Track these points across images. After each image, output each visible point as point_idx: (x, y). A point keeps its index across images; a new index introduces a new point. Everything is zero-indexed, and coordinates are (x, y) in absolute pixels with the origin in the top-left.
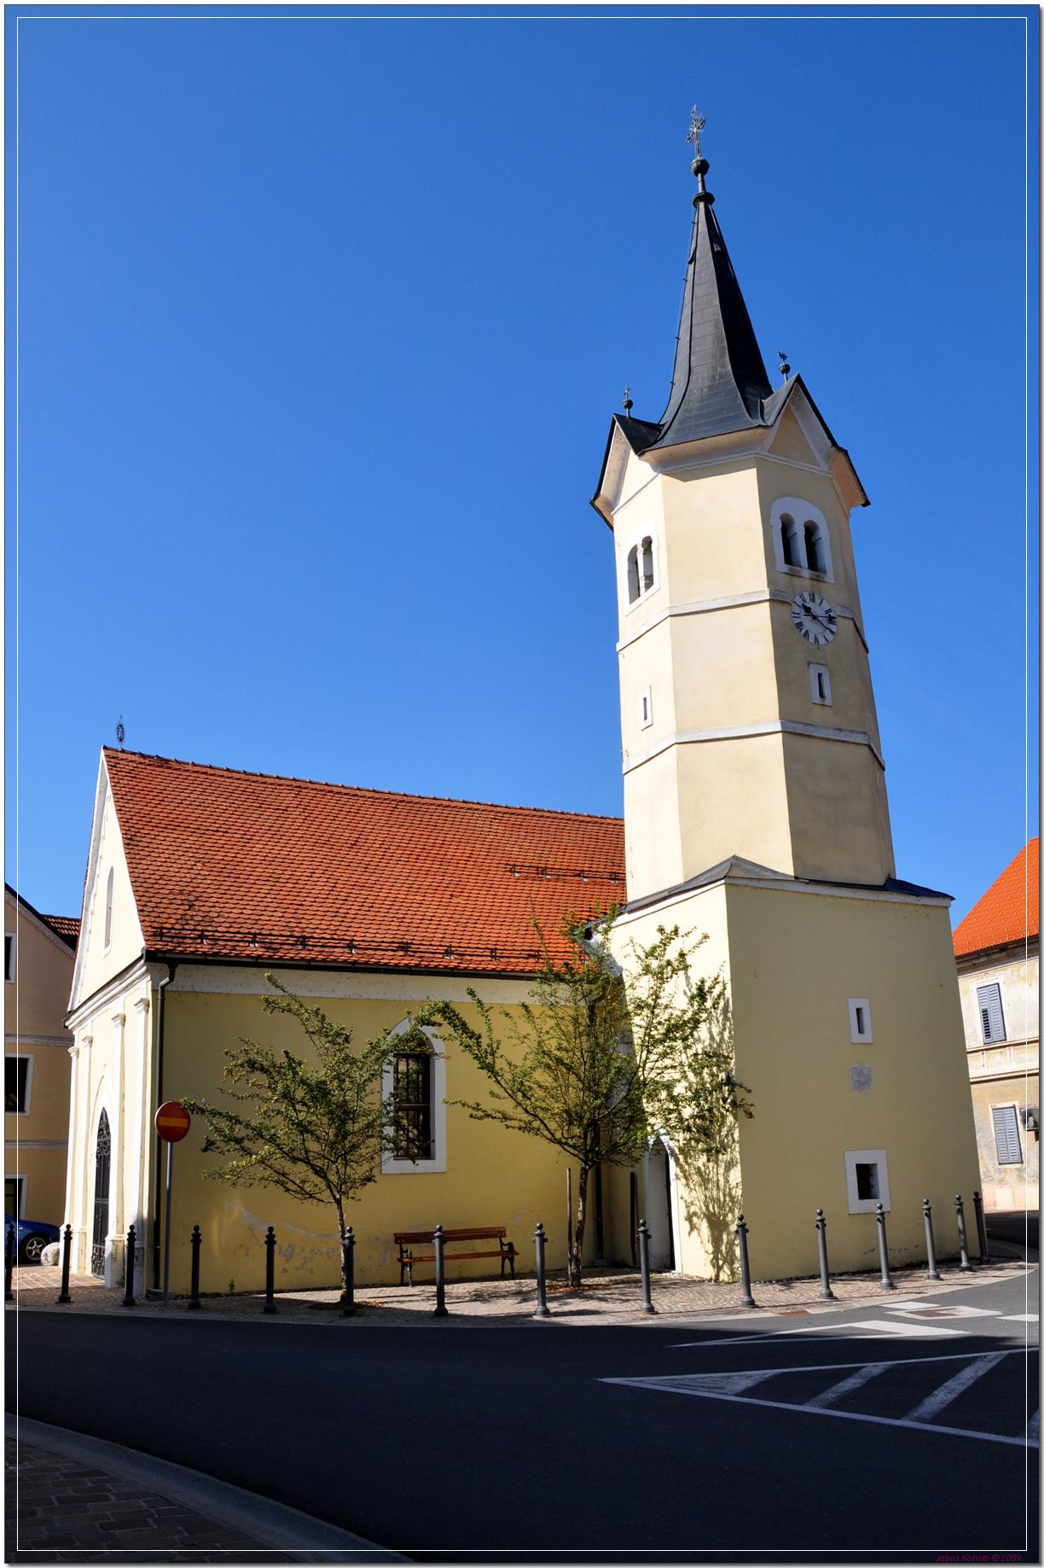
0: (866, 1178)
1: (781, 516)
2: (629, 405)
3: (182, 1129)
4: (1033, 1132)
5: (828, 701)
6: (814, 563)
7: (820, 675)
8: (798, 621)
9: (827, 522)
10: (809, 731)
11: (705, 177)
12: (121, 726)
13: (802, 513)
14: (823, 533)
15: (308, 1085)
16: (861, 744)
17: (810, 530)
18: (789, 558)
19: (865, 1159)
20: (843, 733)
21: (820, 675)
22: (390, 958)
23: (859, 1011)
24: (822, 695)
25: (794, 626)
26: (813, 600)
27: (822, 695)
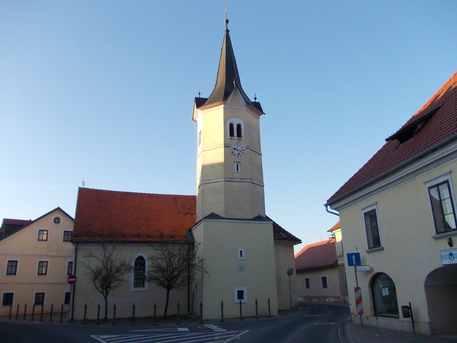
0: (240, 294)
1: (231, 123)
2: (200, 94)
3: (75, 281)
4: (370, 270)
5: (239, 171)
6: (239, 135)
7: (237, 165)
8: (232, 151)
9: (244, 124)
10: (233, 180)
11: (227, 24)
12: (84, 182)
13: (235, 122)
14: (243, 127)
15: (162, 250)
16: (249, 182)
17: (239, 126)
18: (232, 134)
19: (241, 289)
20: (243, 180)
21: (237, 165)
22: (133, 239)
23: (241, 252)
24: (237, 170)
25: (231, 153)
26: (237, 145)
27: (237, 170)
